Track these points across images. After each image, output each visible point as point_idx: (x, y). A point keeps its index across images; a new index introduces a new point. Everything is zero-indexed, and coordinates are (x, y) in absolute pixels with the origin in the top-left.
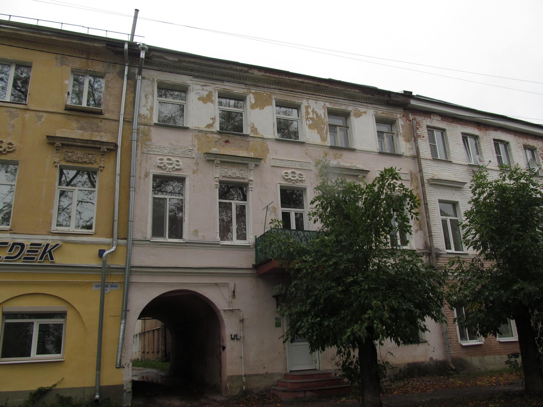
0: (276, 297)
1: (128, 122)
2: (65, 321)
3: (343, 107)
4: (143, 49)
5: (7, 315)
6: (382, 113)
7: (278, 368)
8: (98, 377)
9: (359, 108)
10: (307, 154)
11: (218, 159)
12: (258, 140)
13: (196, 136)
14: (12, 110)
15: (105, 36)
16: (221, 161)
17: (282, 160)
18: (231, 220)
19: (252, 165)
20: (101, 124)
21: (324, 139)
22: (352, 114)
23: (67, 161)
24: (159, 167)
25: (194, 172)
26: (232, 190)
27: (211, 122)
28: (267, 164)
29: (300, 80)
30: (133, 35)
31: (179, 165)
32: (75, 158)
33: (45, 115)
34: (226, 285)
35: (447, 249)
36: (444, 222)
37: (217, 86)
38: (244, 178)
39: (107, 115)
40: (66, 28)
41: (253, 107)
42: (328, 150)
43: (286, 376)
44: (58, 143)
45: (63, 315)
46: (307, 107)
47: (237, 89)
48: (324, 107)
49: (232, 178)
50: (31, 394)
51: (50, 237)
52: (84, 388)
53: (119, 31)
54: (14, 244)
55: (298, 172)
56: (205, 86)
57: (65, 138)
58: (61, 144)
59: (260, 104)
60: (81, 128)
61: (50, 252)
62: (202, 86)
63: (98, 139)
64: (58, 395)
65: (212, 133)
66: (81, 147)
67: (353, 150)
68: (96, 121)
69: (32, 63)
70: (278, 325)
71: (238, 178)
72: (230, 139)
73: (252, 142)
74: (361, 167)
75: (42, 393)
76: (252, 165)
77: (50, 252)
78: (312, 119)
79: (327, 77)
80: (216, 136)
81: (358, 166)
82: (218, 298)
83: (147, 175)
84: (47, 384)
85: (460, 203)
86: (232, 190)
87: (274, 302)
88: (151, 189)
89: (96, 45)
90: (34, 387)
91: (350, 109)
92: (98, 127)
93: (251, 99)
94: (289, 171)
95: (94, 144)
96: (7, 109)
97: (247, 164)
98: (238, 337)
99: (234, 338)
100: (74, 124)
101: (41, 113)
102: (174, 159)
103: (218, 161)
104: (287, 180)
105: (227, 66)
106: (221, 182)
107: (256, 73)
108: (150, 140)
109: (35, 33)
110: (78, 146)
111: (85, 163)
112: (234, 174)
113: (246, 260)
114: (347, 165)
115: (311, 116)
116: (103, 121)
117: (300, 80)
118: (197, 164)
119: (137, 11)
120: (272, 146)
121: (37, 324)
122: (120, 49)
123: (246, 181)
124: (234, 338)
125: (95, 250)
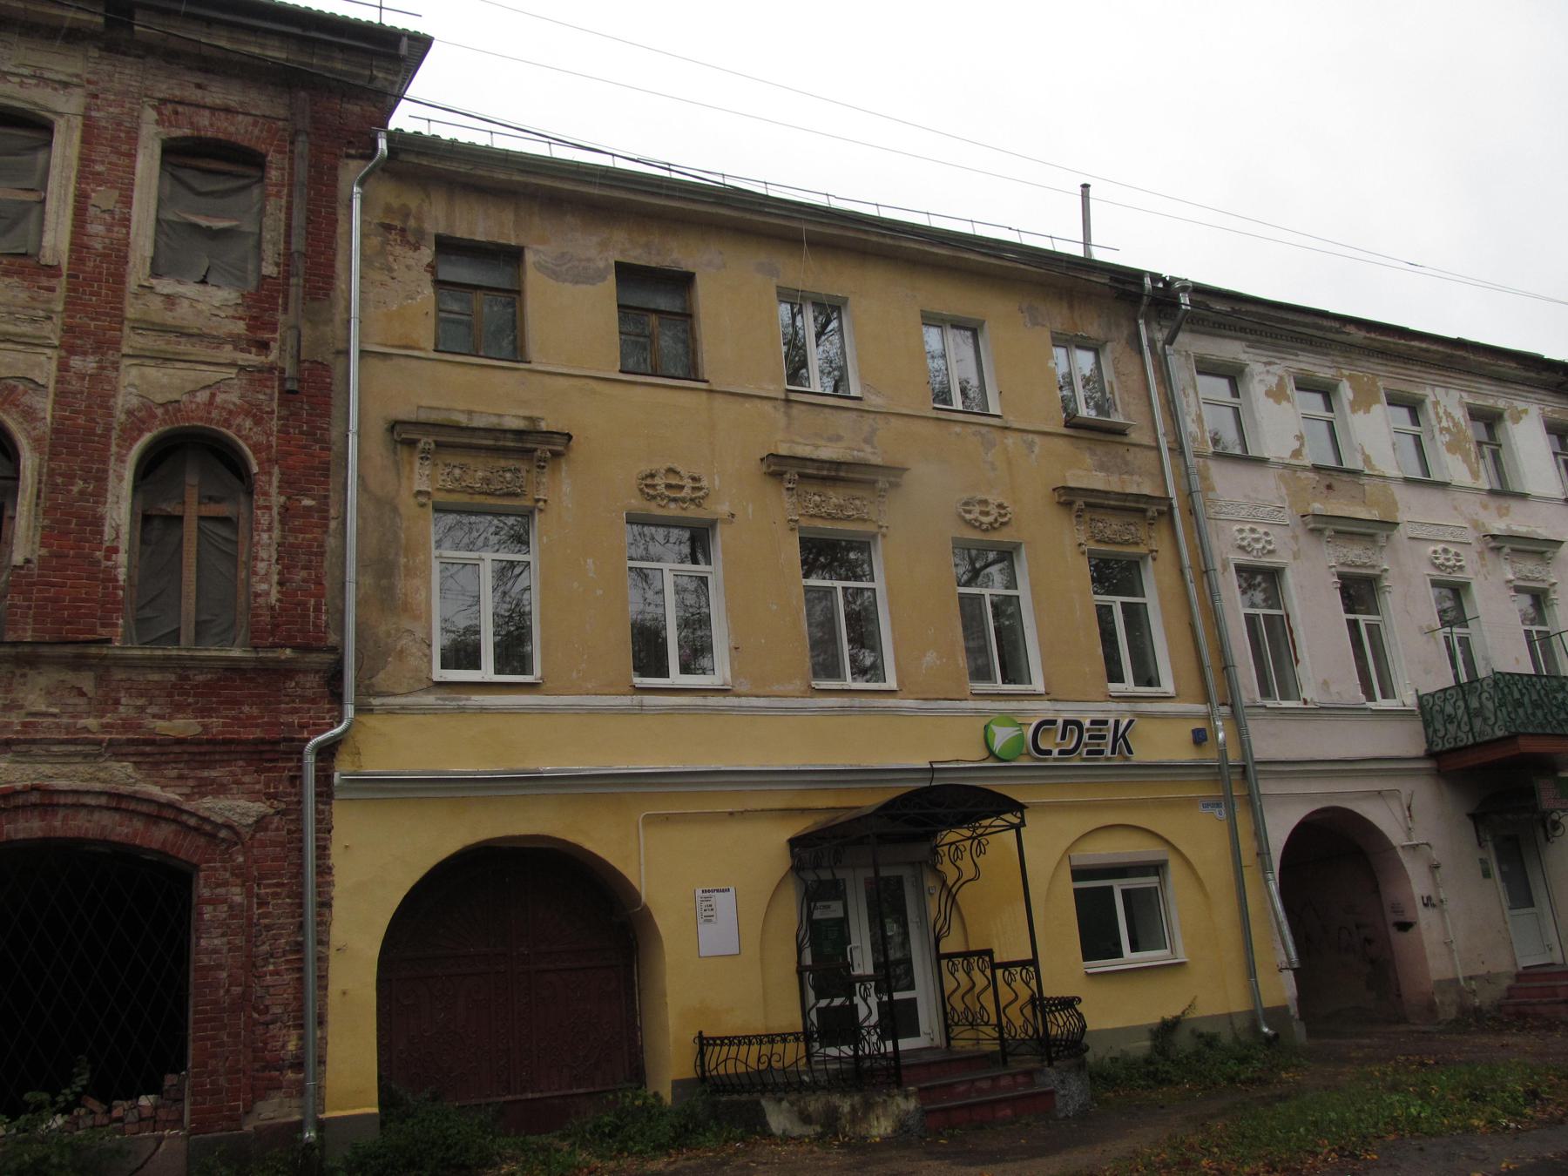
0: (1472, 816)
1: (1178, 449)
2: (1163, 882)
3: (1490, 402)
4: (1184, 289)
5: (1079, 874)
6: (1553, 412)
7: (1502, 964)
8: (1254, 992)
9: (1516, 403)
10: (1456, 509)
11: (794, 471)
12: (1377, 481)
13: (1281, 476)
14: (984, 430)
15: (926, 223)
16: (801, 475)
17: (1423, 524)
18: (1369, 653)
19: (1381, 535)
20: (1129, 457)
21: (1475, 475)
22: (1506, 415)
23: (1098, 541)
24: (1241, 548)
25: (1296, 556)
26: (1359, 592)
27: (1296, 445)
28: (1401, 533)
29: (1424, 345)
30: (1087, 243)
31: (1269, 542)
32: (1108, 532)
33: (1037, 439)
34: (1394, 794)
35: (1111, 680)
36: (1251, 620)
37: (1288, 363)
38: (1373, 567)
39: (1134, 436)
40: (886, 214)
41: (1355, 406)
42: (1486, 499)
43: (1518, 977)
44: (1079, 503)
45: (1157, 868)
46: (1436, 404)
47: (1321, 368)
48: (1460, 402)
49: (1115, 543)
50: (1151, 1031)
51: (1113, 706)
52: (1230, 1015)
53: (1051, 228)
54: (1067, 723)
55: (1453, 549)
56: (1270, 363)
57: (1093, 491)
58: (436, 442)
59: (1363, 401)
60: (1102, 467)
61: (1123, 735)
62: (1266, 364)
63: (1133, 490)
64: (1193, 1031)
65: (1304, 468)
66: (1114, 508)
67: (1523, 496)
68: (1122, 450)
69: (845, 300)
70: (1486, 874)
71: (1364, 566)
72: (1335, 484)
73: (1369, 486)
74: (1544, 533)
75: (1167, 1029)
76: (1381, 535)
77: (1123, 735)
78: (1448, 430)
79: (1453, 335)
80: (1311, 475)
81: (1539, 531)
82: (1385, 818)
83: (1225, 567)
84: (1171, 1011)
85: (1474, 588)
86: (1359, 592)
87: (1470, 823)
88: (1238, 592)
89: (904, 244)
90: (1153, 1018)
91: (1501, 404)
92: (1126, 463)
93: (1346, 392)
94: (1439, 547)
95: (521, 441)
96: (974, 428)
97: (1371, 535)
98: (1434, 901)
99: (1428, 902)
100: (1089, 460)
101: (1030, 436)
102: (1261, 530)
103: (792, 474)
104: (969, 523)
105: (1308, 320)
106: (1341, 576)
107: (1359, 335)
108: (1213, 489)
109: (884, 235)
110: (479, 448)
111: (1126, 543)
112: (1355, 555)
113: (1406, 741)
114: (1522, 530)
115: (1444, 424)
116: (1132, 449)
117: (1424, 345)
118: (1295, 538)
119: (1085, 186)
120: (1402, 494)
121: (1118, 886)
122: (1133, 288)
123: (1376, 572)
124: (1428, 902)
125: (1186, 730)
